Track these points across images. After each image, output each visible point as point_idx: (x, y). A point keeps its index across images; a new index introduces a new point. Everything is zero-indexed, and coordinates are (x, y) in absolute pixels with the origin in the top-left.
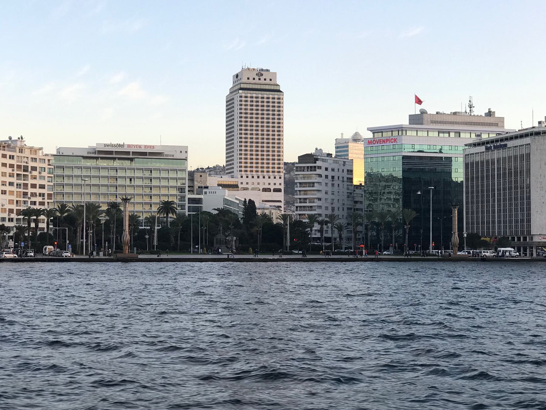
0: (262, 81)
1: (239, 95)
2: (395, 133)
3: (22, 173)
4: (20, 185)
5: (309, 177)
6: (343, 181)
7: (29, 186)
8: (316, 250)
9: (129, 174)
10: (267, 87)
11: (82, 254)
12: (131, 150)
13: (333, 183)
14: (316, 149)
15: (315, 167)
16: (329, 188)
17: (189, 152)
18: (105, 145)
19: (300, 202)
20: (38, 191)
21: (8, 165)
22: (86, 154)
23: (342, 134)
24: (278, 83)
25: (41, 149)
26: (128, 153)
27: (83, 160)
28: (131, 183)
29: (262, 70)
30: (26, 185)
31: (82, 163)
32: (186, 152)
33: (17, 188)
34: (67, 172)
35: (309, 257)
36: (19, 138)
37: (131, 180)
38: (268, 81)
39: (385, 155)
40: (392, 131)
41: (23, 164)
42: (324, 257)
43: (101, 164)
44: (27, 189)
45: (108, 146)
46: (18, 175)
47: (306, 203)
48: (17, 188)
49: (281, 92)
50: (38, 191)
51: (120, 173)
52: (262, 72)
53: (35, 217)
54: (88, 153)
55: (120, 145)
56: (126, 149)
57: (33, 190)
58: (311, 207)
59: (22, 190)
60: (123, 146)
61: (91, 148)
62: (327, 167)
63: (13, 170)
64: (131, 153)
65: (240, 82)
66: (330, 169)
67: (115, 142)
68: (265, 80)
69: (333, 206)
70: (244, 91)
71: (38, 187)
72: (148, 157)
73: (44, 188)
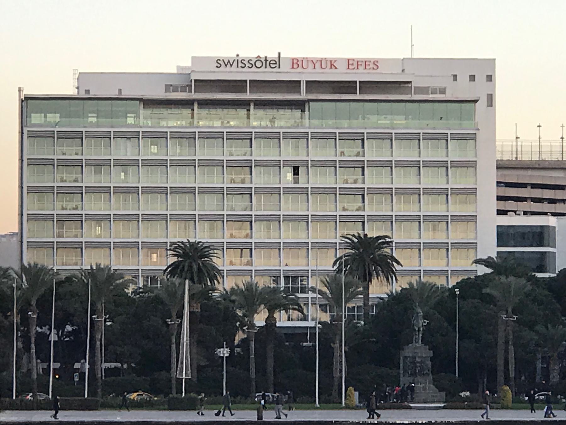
9: (289, 152)
12: (304, 77)
18: (219, 62)
22: (160, 93)
23: (120, 90)
26: (294, 85)
27: (142, 112)
28: (296, 181)
31: (142, 121)
32: (490, 78)
34: (372, 153)
37: (296, 171)
40: (242, 250)
43: (171, 124)
45: (228, 63)
51: (261, 152)
54: (168, 88)
55: (267, 62)
60: (276, 63)
61: (183, 74)
64: (303, 86)
72: (358, 97)
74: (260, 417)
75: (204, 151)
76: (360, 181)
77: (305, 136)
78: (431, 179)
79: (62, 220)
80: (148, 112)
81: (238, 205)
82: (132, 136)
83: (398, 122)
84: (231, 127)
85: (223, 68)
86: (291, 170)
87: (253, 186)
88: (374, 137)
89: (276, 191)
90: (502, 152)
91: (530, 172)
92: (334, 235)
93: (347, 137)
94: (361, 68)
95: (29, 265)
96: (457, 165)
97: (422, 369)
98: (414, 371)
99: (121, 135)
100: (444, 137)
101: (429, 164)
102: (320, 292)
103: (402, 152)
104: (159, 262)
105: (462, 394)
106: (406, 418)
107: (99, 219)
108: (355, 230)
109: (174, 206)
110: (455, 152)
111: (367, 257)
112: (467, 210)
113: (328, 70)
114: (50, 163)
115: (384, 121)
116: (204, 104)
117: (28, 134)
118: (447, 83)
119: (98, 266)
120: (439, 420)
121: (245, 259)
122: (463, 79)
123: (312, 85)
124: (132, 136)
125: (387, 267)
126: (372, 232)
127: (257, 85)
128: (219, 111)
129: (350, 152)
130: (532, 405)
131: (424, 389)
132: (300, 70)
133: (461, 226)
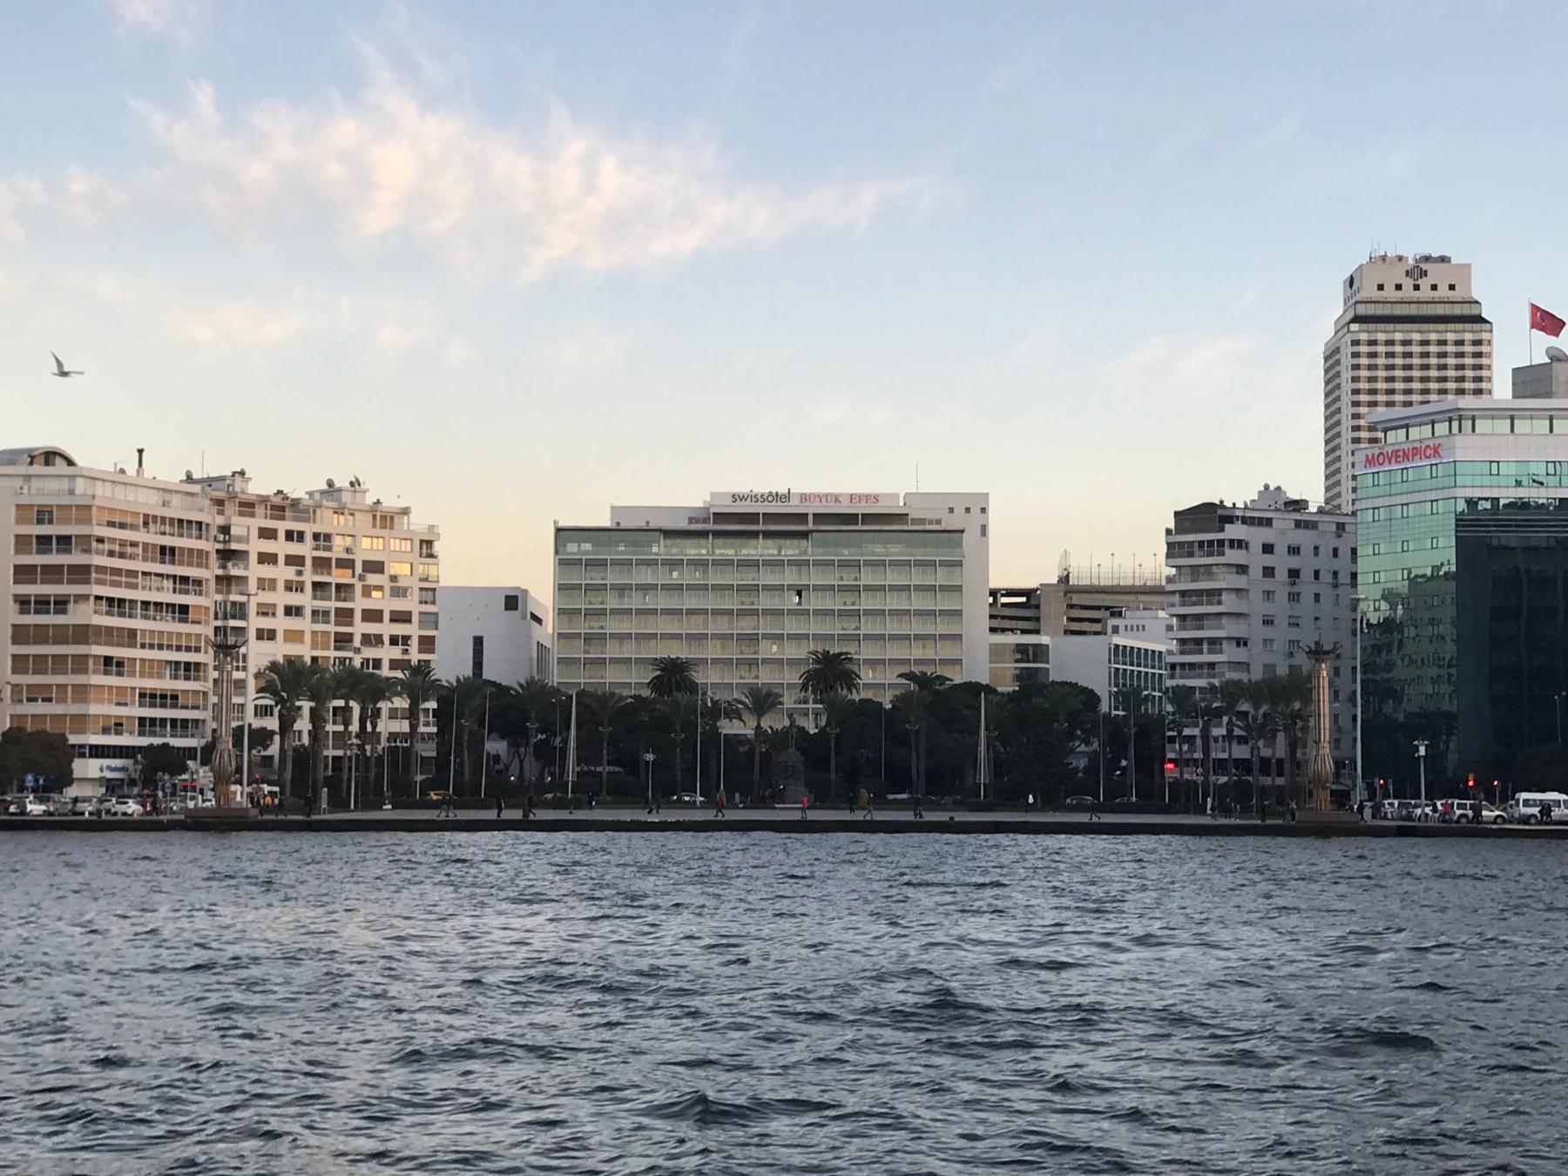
0: (1425, 293)
1: (1349, 338)
2: (1442, 428)
4: (326, 613)
6: (1336, 586)
8: (1185, 797)
9: (791, 577)
10: (1440, 310)
13: (1296, 589)
14: (1267, 487)
15: (1221, 543)
16: (1280, 607)
17: (991, 510)
20: (386, 629)
21: (281, 560)
22: (683, 524)
24: (1476, 297)
25: (405, 512)
26: (802, 517)
29: (1427, 259)
30: (345, 616)
32: (983, 510)
33: (313, 621)
34: (867, 578)
35: (930, 817)
36: (352, 484)
38: (1443, 292)
39: (1411, 498)
44: (351, 624)
45: (743, 498)
46: (316, 585)
47: (1201, 652)
48: (313, 621)
49: (1486, 321)
50: (386, 629)
51: (768, 578)
52: (1424, 266)
53: (340, 703)
54: (691, 520)
55: (777, 497)
56: (793, 507)
57: (372, 628)
58: (1212, 665)
59: (332, 628)
62: (1270, 541)
63: (300, 573)
64: (810, 518)
66: (1281, 549)
67: (762, 488)
68: (1434, 287)
70: (1364, 326)
71: (386, 617)
73: (410, 621)
74: (525, 815)
75: (715, 578)
79: (589, 638)
80: (669, 542)
82: (652, 563)
83: (895, 551)
95: (521, 685)
99: (640, 563)
103: (893, 578)
104: (648, 675)
105: (1471, 777)
107: (622, 638)
110: (942, 577)
111: (830, 672)
112: (953, 629)
114: (830, 563)
115: (879, 549)
117: (564, 563)
118: (944, 515)
124: (652, 563)
125: (849, 679)
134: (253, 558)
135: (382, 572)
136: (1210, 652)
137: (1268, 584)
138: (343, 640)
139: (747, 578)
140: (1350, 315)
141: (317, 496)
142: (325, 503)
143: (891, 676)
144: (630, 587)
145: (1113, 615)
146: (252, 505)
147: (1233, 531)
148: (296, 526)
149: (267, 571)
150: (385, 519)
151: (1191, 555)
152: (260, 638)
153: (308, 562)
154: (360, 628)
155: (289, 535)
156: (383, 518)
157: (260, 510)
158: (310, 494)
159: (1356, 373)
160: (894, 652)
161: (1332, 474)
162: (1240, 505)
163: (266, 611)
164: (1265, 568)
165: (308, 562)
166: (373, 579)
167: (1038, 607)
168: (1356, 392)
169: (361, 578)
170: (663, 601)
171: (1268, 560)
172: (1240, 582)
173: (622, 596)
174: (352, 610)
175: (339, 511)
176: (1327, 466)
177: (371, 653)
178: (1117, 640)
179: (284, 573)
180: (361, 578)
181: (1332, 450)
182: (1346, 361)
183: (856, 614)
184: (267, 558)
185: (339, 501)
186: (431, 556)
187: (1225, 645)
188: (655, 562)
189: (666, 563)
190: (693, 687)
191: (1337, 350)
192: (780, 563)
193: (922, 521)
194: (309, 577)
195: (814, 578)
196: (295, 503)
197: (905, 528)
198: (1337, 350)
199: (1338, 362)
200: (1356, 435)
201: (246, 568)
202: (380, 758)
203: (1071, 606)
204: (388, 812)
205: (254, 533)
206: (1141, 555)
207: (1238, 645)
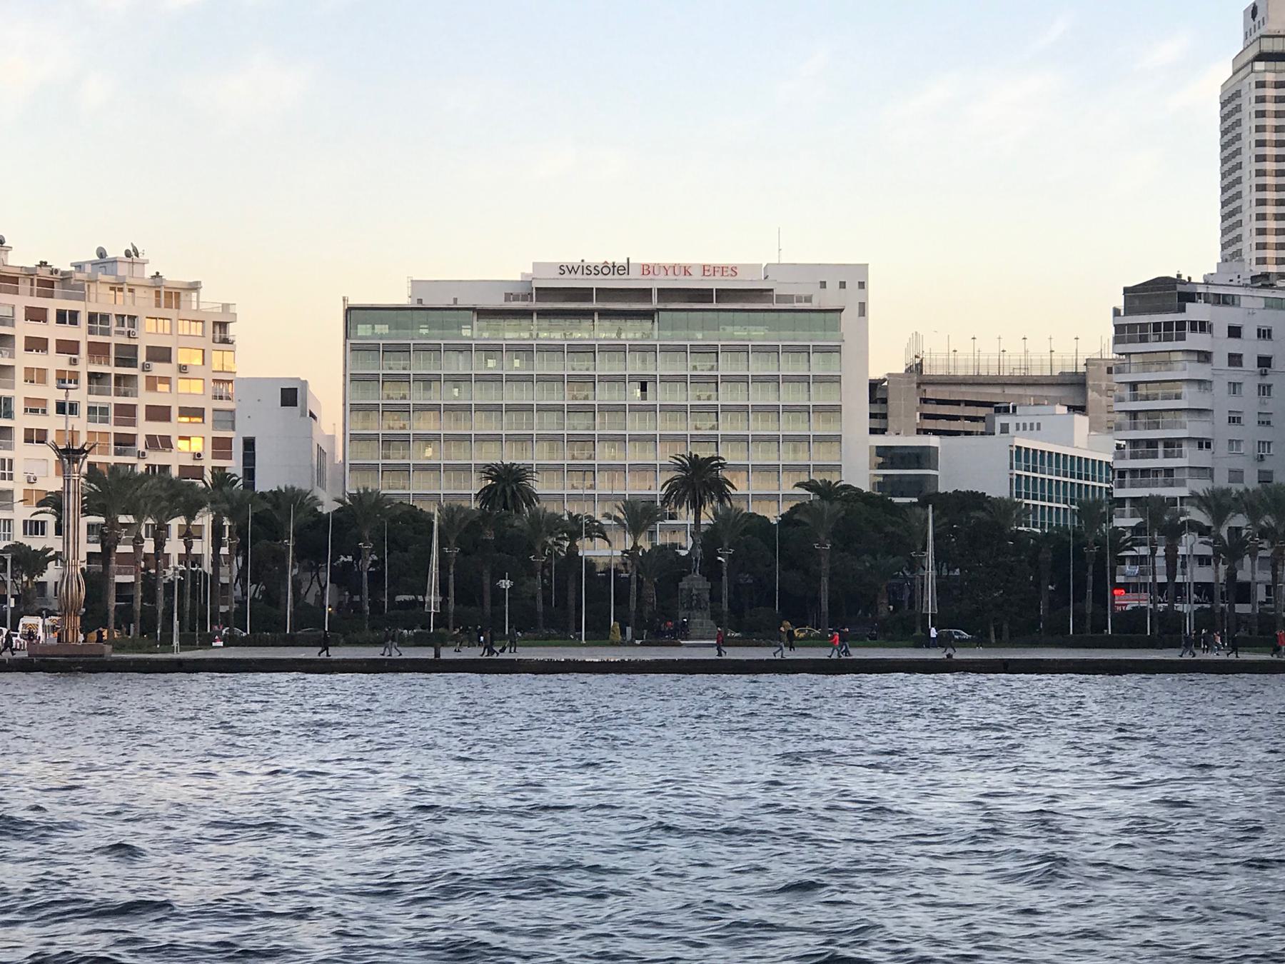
1: (1253, 79)
3: (112, 370)
4: (104, 410)
5: (1165, 360)
7: (141, 413)
9: (635, 366)
11: (167, 641)
13: (1267, 380)
15: (1181, 325)
16: (1248, 402)
19: (1134, 456)
21: (52, 346)
22: (498, 302)
25: (194, 287)
26: (645, 294)
28: (644, 398)
30: (126, 413)
32: (862, 285)
34: (726, 366)
36: (128, 254)
37: (644, 388)
41: (114, 340)
42: (1222, 656)
43: (508, 335)
44: (133, 424)
45: (572, 270)
47: (1155, 456)
51: (604, 366)
54: (508, 297)
55: (614, 269)
56: (634, 281)
58: (1169, 472)
59: (111, 428)
60: (625, 269)
62: (1237, 323)
64: (655, 293)
65: (1263, 31)
66: (1249, 332)
67: (595, 258)
69: (1265, 466)
70: (1271, 65)
72: (714, 306)
74: (437, 655)
75: (541, 366)
76: (714, 397)
77: (652, 349)
78: (791, 395)
79: (388, 441)
80: (483, 323)
81: (578, 425)
82: (465, 349)
83: (758, 334)
84: (421, 336)
85: (567, 275)
86: (638, 385)
87: (596, 403)
88: (730, 349)
89: (621, 409)
90: (967, 367)
91: (963, 389)
92: (663, 455)
93: (699, 350)
94: (718, 275)
96: (820, 380)
97: (698, 601)
98: (693, 604)
100: (805, 350)
101: (789, 379)
102: (616, 519)
103: (758, 366)
104: (476, 485)
106: (596, 656)
108: (680, 450)
109: (507, 425)
110: (818, 366)
111: (699, 479)
113: (682, 277)
116: (543, 314)
117: (355, 349)
118: (814, 290)
119: (366, 489)
120: (633, 659)
121: (588, 483)
122: (833, 285)
123: (665, 294)
124: (465, 349)
125: (720, 489)
126: (704, 453)
127: (605, 293)
128: (561, 322)
129: (702, 366)
130: (473, 642)
131: (702, 624)
132: (651, 276)
133: (823, 447)
134: (20, 343)
135: (169, 361)
136: (1166, 455)
137: (1235, 375)
138: (125, 443)
139: (580, 366)
140: (1253, 52)
141: (88, 268)
142: (101, 277)
143: (787, 485)
144: (437, 378)
145: (998, 410)
146: (15, 280)
147: (1195, 311)
148: (69, 305)
149: (36, 360)
150: (171, 296)
151: (1144, 339)
152: (28, 440)
153: (83, 348)
154: (144, 428)
155: (61, 317)
156: (169, 295)
157: (24, 286)
158: (79, 266)
159: (1261, 121)
160: (788, 456)
161: (1230, 240)
162: (1197, 278)
163: (35, 407)
164: (1230, 355)
165: (83, 348)
166: (159, 369)
167: (885, 401)
168: (1261, 143)
169: (145, 368)
170: (480, 395)
171: (1235, 346)
172: (1202, 371)
173: (427, 388)
174: (133, 407)
175: (116, 287)
176: (1224, 232)
177: (157, 458)
178: (1019, 442)
179: (54, 362)
180: (145, 368)
181: (1230, 214)
182: (1249, 107)
183: (714, 410)
184: (37, 344)
185: (114, 273)
186: (225, 341)
187: (1185, 448)
188: (468, 348)
189: (480, 348)
190: (530, 497)
191: (1238, 94)
192: (621, 349)
193: (788, 298)
194: (85, 367)
195: (664, 366)
196: (66, 277)
197: (771, 306)
198: (1238, 94)
199: (1238, 109)
200: (1261, 195)
201: (12, 356)
202: (169, 586)
203: (925, 401)
204: (219, 651)
205: (20, 314)
206: (1087, 336)
207: (1200, 446)
